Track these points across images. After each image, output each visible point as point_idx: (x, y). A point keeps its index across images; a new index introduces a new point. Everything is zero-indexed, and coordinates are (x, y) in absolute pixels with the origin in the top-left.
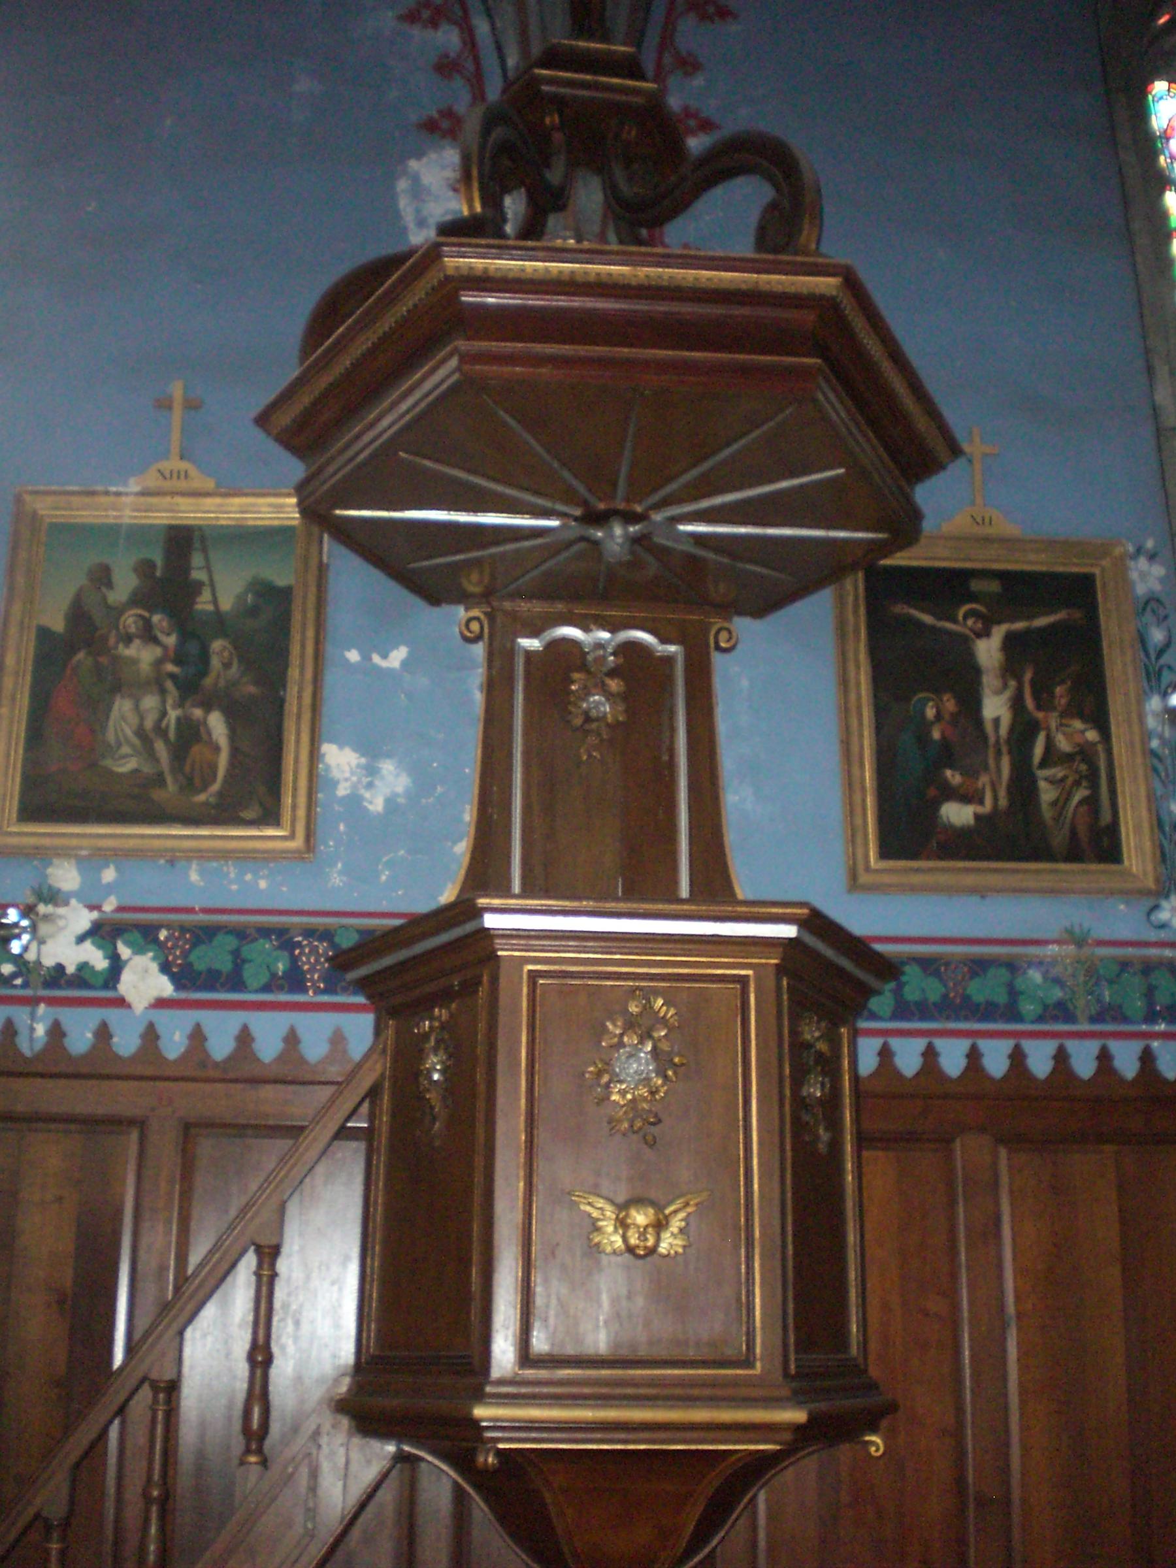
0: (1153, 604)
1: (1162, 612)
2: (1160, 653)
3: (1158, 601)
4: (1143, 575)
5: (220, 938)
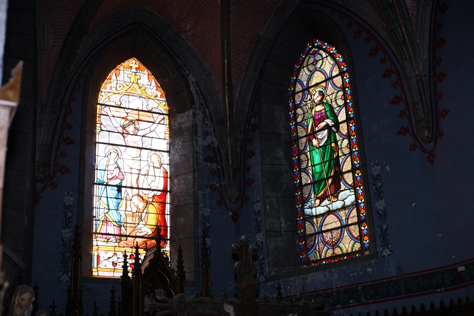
0: (378, 177)
1: (72, 209)
2: (69, 219)
3: (71, 206)
4: (376, 170)
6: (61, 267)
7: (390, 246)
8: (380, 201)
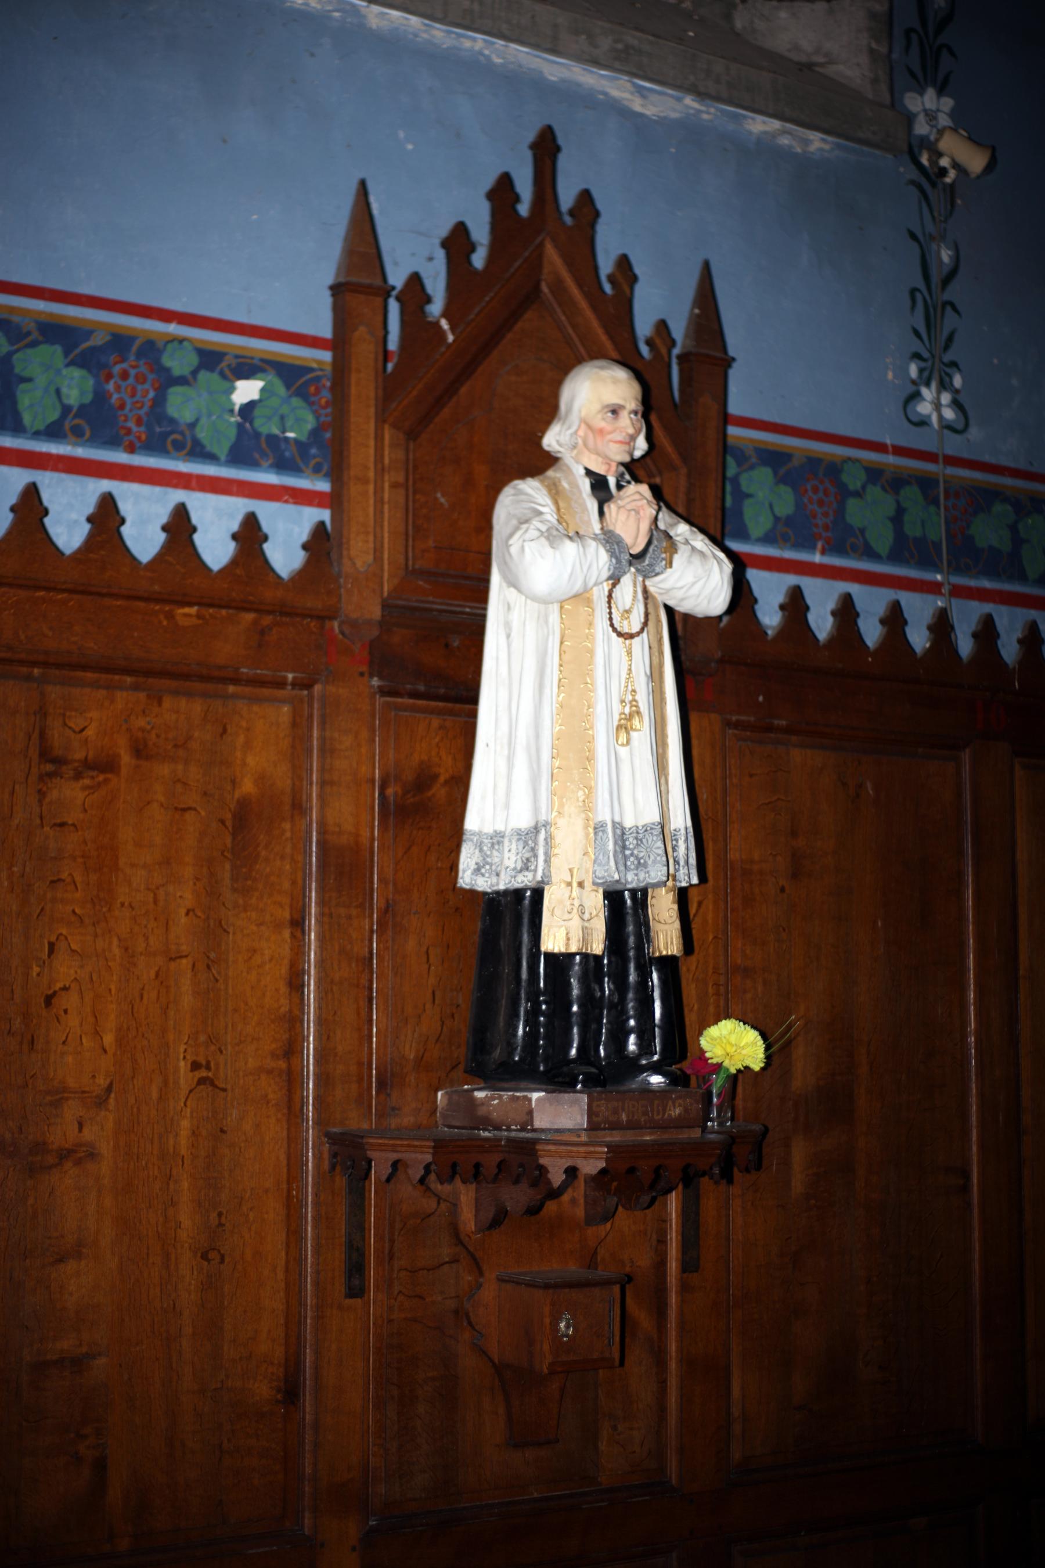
5: (998, 508)
6: (917, 333)
7: (958, 381)
8: (930, 93)
